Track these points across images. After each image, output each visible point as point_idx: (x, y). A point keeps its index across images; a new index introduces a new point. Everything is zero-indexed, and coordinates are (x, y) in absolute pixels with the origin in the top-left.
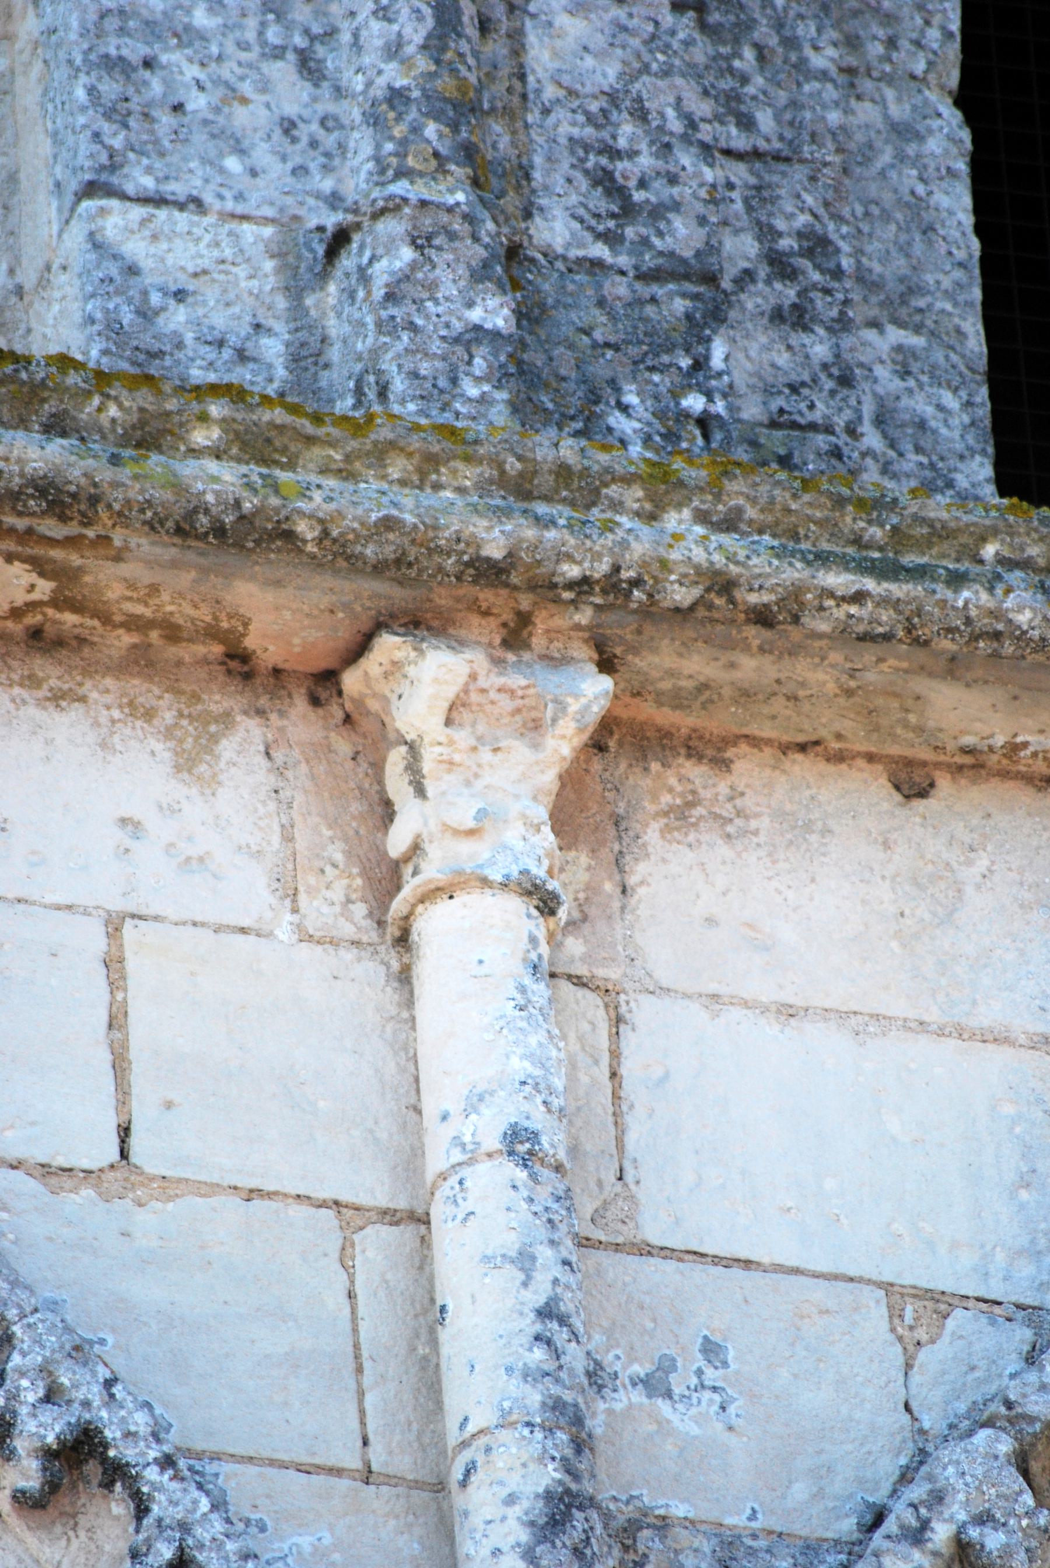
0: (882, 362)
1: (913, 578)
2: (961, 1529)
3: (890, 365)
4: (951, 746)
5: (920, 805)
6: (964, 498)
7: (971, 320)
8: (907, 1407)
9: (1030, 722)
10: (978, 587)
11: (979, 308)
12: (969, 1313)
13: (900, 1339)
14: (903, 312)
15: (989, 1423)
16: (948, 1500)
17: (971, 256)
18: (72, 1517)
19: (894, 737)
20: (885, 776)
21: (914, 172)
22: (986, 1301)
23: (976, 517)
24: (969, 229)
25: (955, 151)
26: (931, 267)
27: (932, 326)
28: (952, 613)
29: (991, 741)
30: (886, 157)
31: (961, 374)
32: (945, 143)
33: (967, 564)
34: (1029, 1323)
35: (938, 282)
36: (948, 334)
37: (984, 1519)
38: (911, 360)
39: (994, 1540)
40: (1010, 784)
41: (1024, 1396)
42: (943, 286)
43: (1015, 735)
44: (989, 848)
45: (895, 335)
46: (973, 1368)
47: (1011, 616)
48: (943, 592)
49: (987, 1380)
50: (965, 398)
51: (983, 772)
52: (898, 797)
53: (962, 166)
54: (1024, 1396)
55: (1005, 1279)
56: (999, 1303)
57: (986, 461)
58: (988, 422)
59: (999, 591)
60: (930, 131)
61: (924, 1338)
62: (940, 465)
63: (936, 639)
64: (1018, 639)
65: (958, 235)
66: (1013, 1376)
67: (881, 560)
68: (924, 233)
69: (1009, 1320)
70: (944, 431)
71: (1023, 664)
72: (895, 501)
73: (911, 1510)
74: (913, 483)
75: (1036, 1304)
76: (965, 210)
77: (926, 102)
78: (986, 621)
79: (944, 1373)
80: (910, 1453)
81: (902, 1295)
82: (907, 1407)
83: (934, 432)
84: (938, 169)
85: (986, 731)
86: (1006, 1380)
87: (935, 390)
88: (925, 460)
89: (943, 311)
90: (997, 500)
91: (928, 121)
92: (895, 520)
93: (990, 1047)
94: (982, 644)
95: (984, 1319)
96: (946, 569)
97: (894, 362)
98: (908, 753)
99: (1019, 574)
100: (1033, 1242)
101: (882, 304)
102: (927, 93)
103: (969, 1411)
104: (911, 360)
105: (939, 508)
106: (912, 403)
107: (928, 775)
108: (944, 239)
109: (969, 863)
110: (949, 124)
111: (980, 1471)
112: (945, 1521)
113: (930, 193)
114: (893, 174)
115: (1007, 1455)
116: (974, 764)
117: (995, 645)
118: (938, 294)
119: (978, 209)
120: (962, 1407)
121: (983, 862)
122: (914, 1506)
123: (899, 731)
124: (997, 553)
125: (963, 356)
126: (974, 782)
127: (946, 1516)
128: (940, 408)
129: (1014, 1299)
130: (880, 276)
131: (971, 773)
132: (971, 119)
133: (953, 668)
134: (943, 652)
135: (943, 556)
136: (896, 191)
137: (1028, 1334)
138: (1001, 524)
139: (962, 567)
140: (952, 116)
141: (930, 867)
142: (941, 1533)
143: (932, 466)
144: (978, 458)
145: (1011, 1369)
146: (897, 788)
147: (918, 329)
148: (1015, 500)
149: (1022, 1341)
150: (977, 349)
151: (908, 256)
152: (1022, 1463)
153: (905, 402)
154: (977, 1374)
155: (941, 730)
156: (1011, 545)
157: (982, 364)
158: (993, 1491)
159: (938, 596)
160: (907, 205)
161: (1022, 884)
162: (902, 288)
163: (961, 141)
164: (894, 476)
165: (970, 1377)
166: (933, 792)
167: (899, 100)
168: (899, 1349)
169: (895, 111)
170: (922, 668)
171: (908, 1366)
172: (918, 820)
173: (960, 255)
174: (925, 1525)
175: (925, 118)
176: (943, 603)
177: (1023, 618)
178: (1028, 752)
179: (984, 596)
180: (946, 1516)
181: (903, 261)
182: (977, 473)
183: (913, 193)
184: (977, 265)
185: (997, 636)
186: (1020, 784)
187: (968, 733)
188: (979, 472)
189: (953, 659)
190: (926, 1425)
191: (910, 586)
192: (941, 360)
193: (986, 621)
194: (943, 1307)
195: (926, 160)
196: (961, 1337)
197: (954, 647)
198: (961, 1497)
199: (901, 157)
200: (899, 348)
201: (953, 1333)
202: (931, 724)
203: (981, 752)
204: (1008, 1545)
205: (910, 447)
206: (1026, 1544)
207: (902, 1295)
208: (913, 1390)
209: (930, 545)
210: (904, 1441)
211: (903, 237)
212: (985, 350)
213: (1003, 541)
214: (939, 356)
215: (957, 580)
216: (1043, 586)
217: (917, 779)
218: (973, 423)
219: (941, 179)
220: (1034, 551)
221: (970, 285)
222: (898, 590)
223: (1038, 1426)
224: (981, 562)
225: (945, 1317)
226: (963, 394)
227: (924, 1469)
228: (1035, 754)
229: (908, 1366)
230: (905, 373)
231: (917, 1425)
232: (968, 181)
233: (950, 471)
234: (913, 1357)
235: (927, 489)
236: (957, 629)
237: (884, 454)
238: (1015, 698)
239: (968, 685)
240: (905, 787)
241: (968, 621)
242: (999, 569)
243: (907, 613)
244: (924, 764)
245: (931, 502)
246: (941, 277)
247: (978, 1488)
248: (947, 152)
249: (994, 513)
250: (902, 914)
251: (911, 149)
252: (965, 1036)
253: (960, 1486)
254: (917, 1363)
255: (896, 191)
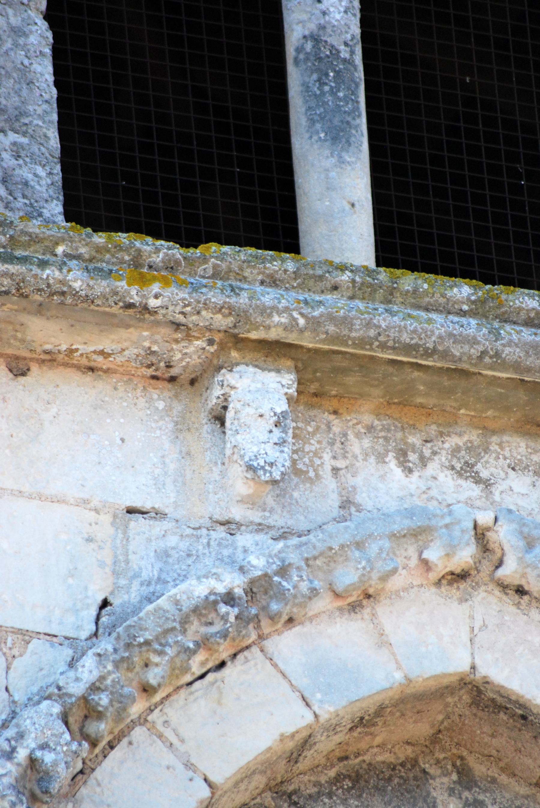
0: (6, 150)
1: (21, 263)
2: (32, 751)
3: (10, 153)
4: (39, 350)
5: (22, 380)
6: (47, 222)
7: (52, 130)
8: (7, 689)
9: (79, 339)
10: (53, 268)
11: (56, 124)
12: (41, 641)
13: (4, 654)
14: (17, 125)
15: (49, 697)
16: (26, 737)
17: (52, 97)
18: (197, 802)
19: (9, 344)
20: (4, 364)
21: (23, 53)
22: (49, 635)
23: (53, 232)
24: (51, 84)
25: (44, 43)
26: (32, 102)
27: (32, 133)
28: (40, 281)
29: (59, 348)
30: (9, 44)
31: (46, 158)
32: (39, 39)
33: (48, 256)
34: (71, 646)
35: (35, 110)
36: (40, 137)
37: (44, 747)
38: (21, 150)
39: (48, 758)
40: (68, 370)
41: (67, 684)
42: (37, 113)
43: (72, 345)
44: (57, 403)
45: (13, 137)
46: (41, 670)
47: (70, 283)
48: (36, 270)
49: (48, 676)
50: (49, 170)
51: (55, 363)
52: (11, 375)
53: (48, 51)
54: (67, 684)
55: (59, 624)
56: (56, 636)
57: (59, 203)
58: (60, 183)
59: (65, 271)
60: (31, 32)
61: (17, 654)
62: (36, 204)
63: (32, 294)
64: (74, 295)
65: (45, 86)
66: (62, 674)
67: (4, 253)
68: (28, 84)
69: (61, 645)
70: (37, 187)
71: (76, 308)
72: (12, 222)
73: (7, 742)
74: (21, 214)
75: (75, 636)
76: (49, 73)
77: (29, 17)
78: (58, 286)
79: (26, 672)
80: (8, 712)
81: (6, 632)
82: (7, 689)
83: (32, 187)
84: (35, 52)
85: (57, 343)
86: (58, 676)
87: (33, 166)
88: (27, 202)
89: (37, 125)
90: (64, 224)
91: (30, 27)
92: (12, 233)
93: (56, 505)
94: (55, 298)
95: (48, 644)
96: (38, 258)
97: (12, 151)
98: (16, 352)
99: (75, 262)
100: (74, 605)
101: (6, 121)
102: (30, 12)
103: (39, 691)
104: (21, 150)
105: (34, 227)
106: (21, 172)
107: (26, 364)
108: (38, 88)
109: (47, 410)
110: (41, 29)
111: (43, 722)
112: (24, 748)
113: (31, 64)
114: (12, 53)
115: (57, 714)
116: (50, 359)
117: (62, 298)
118: (35, 117)
119: (57, 72)
120: (35, 689)
121: (54, 410)
122: (8, 740)
123: (12, 341)
124: (64, 251)
125: (48, 149)
126: (50, 369)
127: (25, 745)
128: (35, 175)
129: (64, 634)
130: (5, 106)
131: (49, 364)
132: (52, 27)
133: (40, 309)
134: (35, 301)
135: (36, 252)
136: (13, 62)
137: (70, 652)
138: (66, 236)
139: (47, 257)
140: (42, 25)
141: (27, 411)
142: (22, 754)
143: (31, 205)
144: (55, 202)
145: (61, 670)
146: (11, 371)
147: (24, 134)
148: (73, 224)
149: (67, 656)
150: (55, 145)
151: (20, 96)
152: (65, 719)
153: (17, 172)
154: (44, 672)
155: (34, 341)
156: (71, 247)
157: (58, 153)
158: (49, 732)
159: (33, 272)
160: (19, 69)
161: (74, 421)
162: (17, 113)
163: (47, 38)
164: (11, 210)
165: (40, 674)
166: (29, 373)
167: (15, 15)
168: (4, 659)
169: (14, 21)
170: (25, 309)
171: (8, 668)
172: (21, 387)
173: (46, 96)
174: (13, 750)
175: (28, 25)
176: (36, 276)
177: (77, 285)
178: (78, 354)
179: (57, 273)
180: (25, 745)
181: (17, 99)
182: (54, 209)
183: (22, 63)
184: (55, 102)
185: (63, 293)
186: (74, 370)
187: (48, 343)
188: (55, 208)
189: (40, 305)
190: (16, 698)
191: (19, 267)
192: (37, 150)
193: (58, 286)
194: (27, 638)
195: (29, 47)
196: (36, 653)
197: (41, 299)
198: (33, 735)
199: (16, 45)
200: (14, 144)
201: (32, 651)
202: (29, 338)
203: (54, 353)
204: (56, 760)
205: (20, 195)
206: (65, 759)
207: (6, 632)
208: (10, 680)
209: (29, 246)
210: (4, 707)
211: (17, 86)
212: (59, 146)
213: (67, 244)
214: (35, 148)
215: (43, 264)
216: (87, 269)
217: (21, 366)
218: (52, 184)
219: (37, 57)
220: (83, 250)
221: (52, 112)
222: (13, 268)
223: (74, 699)
224: (56, 255)
225: (28, 643)
226: (48, 168)
227: (14, 721)
228: (82, 355)
229: (8, 668)
230: (18, 157)
231: (11, 699)
232: (51, 58)
233: (40, 208)
234: (11, 664)
235: (29, 217)
236: (43, 289)
237: (6, 198)
238: (72, 326)
239: (48, 319)
240: (15, 370)
241: (49, 286)
242: (65, 259)
243: (17, 281)
244: (25, 359)
245: (30, 224)
246: (36, 107)
247: (42, 731)
248: (40, 42)
249: (62, 231)
250: (12, 436)
251: (21, 41)
252: (43, 499)
253: (32, 729)
254: (13, 666)
255: (13, 62)
